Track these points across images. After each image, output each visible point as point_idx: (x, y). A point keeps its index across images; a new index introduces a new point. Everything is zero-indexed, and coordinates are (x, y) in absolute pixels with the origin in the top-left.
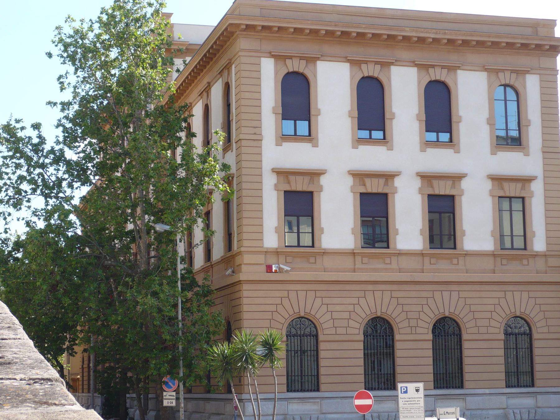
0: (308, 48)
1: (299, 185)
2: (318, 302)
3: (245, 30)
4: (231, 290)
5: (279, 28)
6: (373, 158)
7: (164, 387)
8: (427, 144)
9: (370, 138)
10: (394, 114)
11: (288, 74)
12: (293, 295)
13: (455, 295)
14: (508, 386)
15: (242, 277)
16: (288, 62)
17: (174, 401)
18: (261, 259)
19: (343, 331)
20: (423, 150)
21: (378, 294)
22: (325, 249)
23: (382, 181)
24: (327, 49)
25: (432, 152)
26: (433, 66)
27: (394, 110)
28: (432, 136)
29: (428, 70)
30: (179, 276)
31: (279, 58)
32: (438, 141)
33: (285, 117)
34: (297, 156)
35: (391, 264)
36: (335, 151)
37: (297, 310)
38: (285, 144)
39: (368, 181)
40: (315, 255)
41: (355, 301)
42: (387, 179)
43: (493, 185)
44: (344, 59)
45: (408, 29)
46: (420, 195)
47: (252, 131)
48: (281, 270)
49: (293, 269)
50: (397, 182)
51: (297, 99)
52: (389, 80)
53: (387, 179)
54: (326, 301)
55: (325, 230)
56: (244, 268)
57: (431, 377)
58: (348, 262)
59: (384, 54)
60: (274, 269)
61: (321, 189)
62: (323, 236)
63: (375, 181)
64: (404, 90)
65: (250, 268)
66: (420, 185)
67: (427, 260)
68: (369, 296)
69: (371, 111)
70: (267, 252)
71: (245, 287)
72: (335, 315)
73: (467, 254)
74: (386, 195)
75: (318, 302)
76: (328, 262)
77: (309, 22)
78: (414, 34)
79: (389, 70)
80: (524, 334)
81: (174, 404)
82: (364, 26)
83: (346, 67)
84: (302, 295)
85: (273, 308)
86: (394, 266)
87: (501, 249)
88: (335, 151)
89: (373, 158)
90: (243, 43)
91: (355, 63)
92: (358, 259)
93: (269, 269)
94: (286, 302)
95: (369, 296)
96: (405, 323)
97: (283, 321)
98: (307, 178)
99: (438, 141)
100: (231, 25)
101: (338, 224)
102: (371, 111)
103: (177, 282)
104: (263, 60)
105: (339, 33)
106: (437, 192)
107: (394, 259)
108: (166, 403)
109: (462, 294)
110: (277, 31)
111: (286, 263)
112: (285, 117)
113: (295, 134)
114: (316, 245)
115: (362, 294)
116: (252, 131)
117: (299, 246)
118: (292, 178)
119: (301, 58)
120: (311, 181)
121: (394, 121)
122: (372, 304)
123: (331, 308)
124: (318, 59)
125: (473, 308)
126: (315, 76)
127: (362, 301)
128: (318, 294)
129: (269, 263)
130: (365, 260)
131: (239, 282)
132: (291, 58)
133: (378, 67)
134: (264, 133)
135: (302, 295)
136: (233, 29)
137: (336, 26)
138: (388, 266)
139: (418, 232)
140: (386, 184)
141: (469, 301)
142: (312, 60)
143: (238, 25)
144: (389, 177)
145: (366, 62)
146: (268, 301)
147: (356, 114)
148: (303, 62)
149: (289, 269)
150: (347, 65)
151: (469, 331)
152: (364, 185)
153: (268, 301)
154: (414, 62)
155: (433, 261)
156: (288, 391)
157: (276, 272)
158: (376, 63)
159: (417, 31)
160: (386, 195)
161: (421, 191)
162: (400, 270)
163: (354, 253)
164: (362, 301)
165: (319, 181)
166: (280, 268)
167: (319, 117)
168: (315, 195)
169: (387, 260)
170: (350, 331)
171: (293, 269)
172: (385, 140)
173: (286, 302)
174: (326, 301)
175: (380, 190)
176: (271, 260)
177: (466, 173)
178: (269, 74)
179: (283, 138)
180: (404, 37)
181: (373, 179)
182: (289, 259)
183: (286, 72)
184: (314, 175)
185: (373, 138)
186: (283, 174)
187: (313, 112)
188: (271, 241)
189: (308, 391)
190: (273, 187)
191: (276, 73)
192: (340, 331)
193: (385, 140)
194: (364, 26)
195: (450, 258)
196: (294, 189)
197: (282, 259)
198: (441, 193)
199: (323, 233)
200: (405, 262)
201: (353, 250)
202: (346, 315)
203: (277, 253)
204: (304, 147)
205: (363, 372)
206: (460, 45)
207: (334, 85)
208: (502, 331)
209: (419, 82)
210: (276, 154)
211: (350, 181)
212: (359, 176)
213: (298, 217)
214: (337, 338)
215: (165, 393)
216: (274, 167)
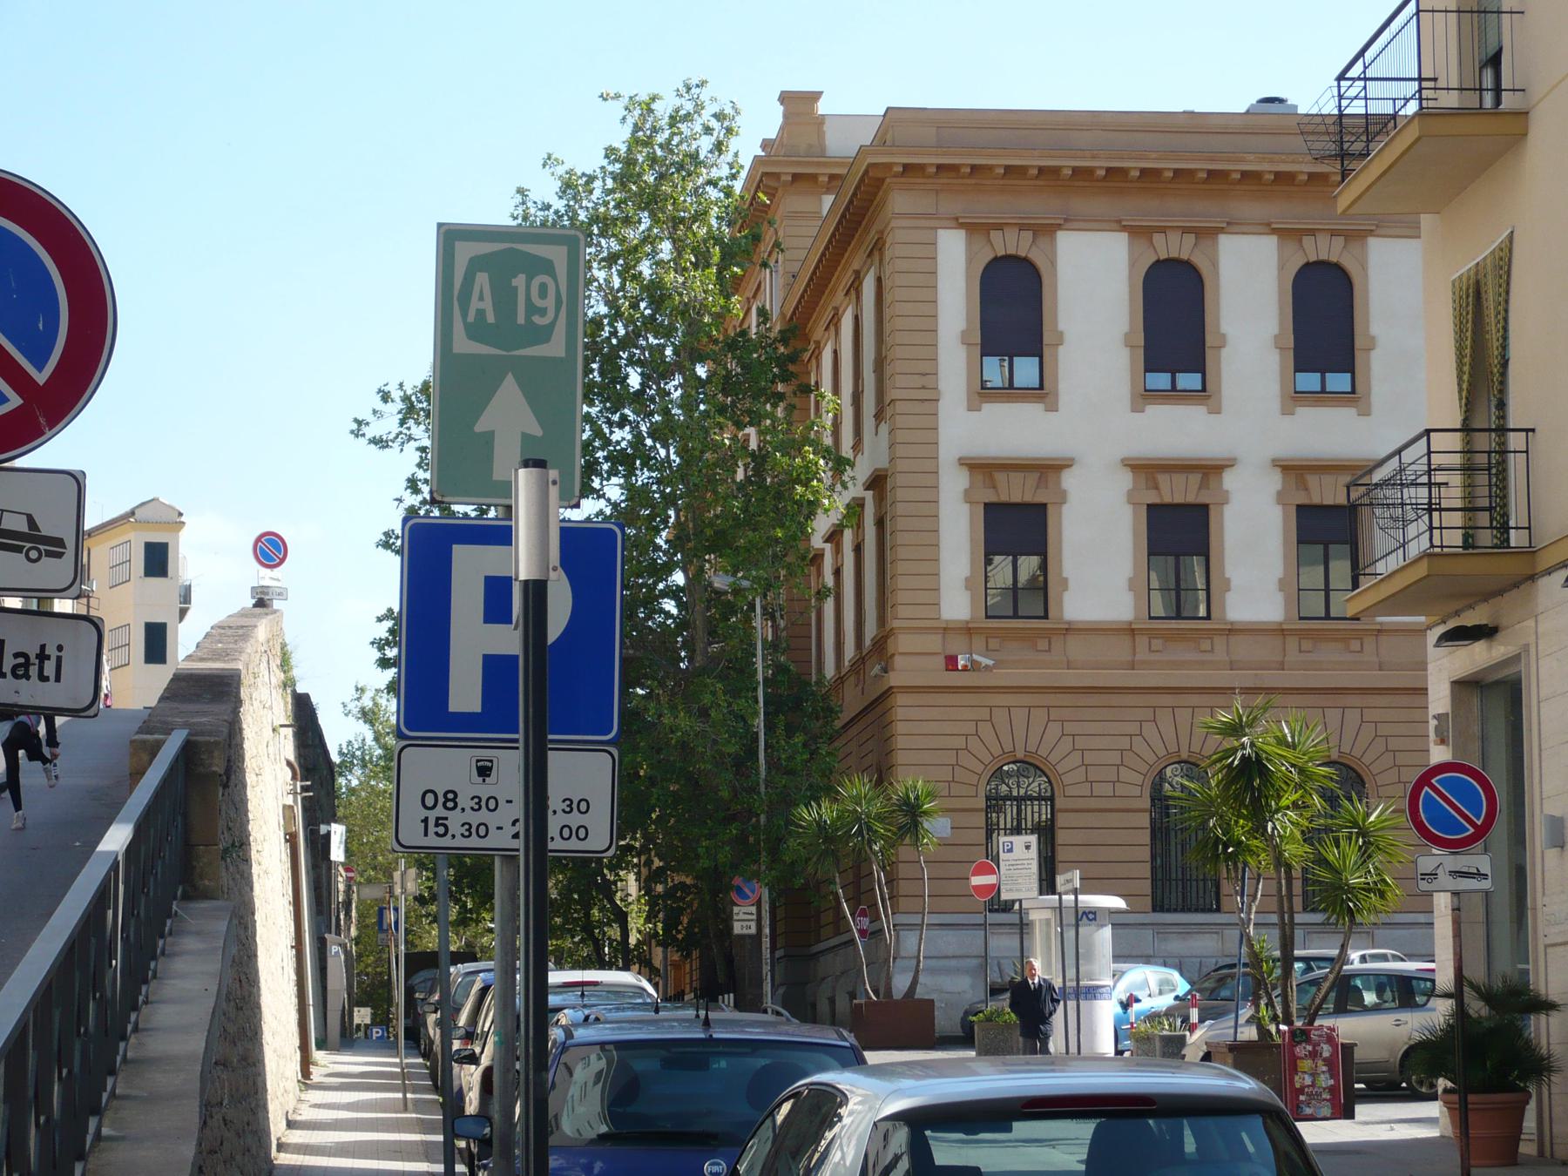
0: (1036, 206)
1: (1016, 491)
2: (1054, 730)
3: (903, 174)
4: (878, 706)
5: (974, 168)
6: (1176, 431)
7: (733, 896)
8: (1296, 398)
9: (1174, 388)
10: (1224, 336)
11: (1158, 263)
12: (1000, 717)
13: (1353, 717)
14: (1158, 907)
15: (894, 679)
16: (995, 236)
17: (753, 925)
18: (933, 643)
19: (1107, 789)
20: (1287, 411)
21: (1184, 715)
22: (1069, 623)
23: (1195, 479)
24: (1079, 205)
25: (1309, 415)
26: (1312, 232)
27: (1225, 327)
28: (1310, 381)
29: (1300, 241)
30: (760, 677)
31: (975, 229)
32: (1323, 391)
33: (987, 350)
34: (1014, 431)
35: (1212, 651)
36: (1093, 417)
37: (1008, 747)
38: (986, 407)
39: (1312, 480)
40: (1049, 634)
41: (1133, 728)
42: (1206, 477)
43: (1135, 482)
44: (1115, 225)
45: (1252, 157)
46: (967, 506)
47: (919, 381)
48: (974, 667)
49: (999, 664)
50: (1230, 480)
51: (1014, 314)
52: (1215, 264)
53: (1206, 477)
54: (1069, 728)
55: (1071, 584)
56: (898, 661)
57: (1146, 886)
58: (1119, 649)
59: (1204, 210)
60: (961, 663)
61: (1062, 497)
62: (1067, 597)
63: (1179, 479)
64: (1248, 287)
65: (913, 663)
66: (1279, 486)
67: (1142, 642)
68: (1165, 719)
69: (1174, 329)
70: (947, 630)
71: (901, 699)
72: (1090, 758)
73: (1070, 630)
74: (1204, 508)
75: (1054, 730)
76: (1075, 648)
77: (1036, 153)
78: (1265, 167)
79: (1364, 247)
80: (1040, 798)
81: (753, 931)
82: (1154, 155)
83: (1269, 244)
84: (1019, 716)
85: (959, 742)
86: (1220, 654)
87: (987, 617)
88: (1093, 417)
89: (1176, 431)
90: (900, 202)
91: (1139, 233)
92: (1142, 642)
93: (951, 662)
94: (986, 730)
95: (1165, 719)
96: (1079, 775)
97: (979, 768)
98: (1033, 478)
99: (1323, 391)
100: (871, 165)
101: (1099, 567)
102: (1174, 329)
103: (755, 689)
104: (941, 232)
105: (1103, 173)
106: (1316, 500)
107: (1219, 642)
108: (738, 929)
109: (1370, 715)
110: (1037, 177)
111: (988, 651)
112: (987, 350)
113: (1011, 386)
114: (1213, 615)
115: (1149, 714)
116: (919, 381)
117: (1328, 617)
118: (1000, 477)
119: (1022, 227)
120: (1042, 482)
121: (1225, 352)
122: (1020, 734)
123: (1081, 743)
124: (1059, 227)
125: (1394, 744)
126: (1053, 263)
127: (1149, 730)
128: (1054, 713)
129: (950, 652)
130: (1157, 644)
131: (889, 692)
132: (1000, 227)
133: (1190, 239)
134: (942, 386)
135: (1019, 716)
136: (880, 175)
137: (1094, 157)
138: (1208, 657)
139: (1273, 586)
140: (1204, 485)
141: (1384, 730)
142: (1045, 231)
143: (889, 166)
144: (1210, 470)
145: (1162, 230)
146: (948, 728)
147: (1140, 340)
148: (1027, 236)
149: (990, 663)
150: (1124, 236)
151: (1070, 791)
152: (1157, 488)
153: (948, 728)
154: (1269, 224)
155: (1306, 645)
156: (1154, 910)
157: (965, 669)
158: (1186, 230)
159: (1271, 161)
160: (1204, 508)
161: (1281, 498)
162: (1232, 666)
163: (1133, 630)
164: (1149, 730)
165: (1058, 483)
166: (973, 662)
167: (1061, 348)
168: (1050, 510)
169: (1206, 645)
170: (1121, 790)
171: (999, 664)
172: (1203, 394)
173: (986, 730)
174: (1069, 728)
175: (1191, 499)
176: (956, 645)
177: (1068, 454)
178: (954, 266)
179: (984, 393)
180: (1245, 174)
181: (1012, 475)
182: (993, 643)
183: (1154, 259)
184: (1049, 469)
185: (1179, 387)
186: (983, 469)
187: (1047, 338)
188: (957, 605)
189: (1196, 911)
190: (961, 495)
191: (970, 261)
192: (1100, 789)
193: (1353, 396)
194: (1154, 155)
195: (1030, 638)
196: (1004, 498)
197: (979, 642)
198: (1326, 502)
199: (1066, 589)
200: (1243, 649)
201: (1131, 623)
202: (1115, 758)
203: (968, 630)
204: (1028, 412)
205: (1148, 875)
206: (1306, 184)
207: (1094, 281)
208: (1147, 794)
209: (1282, 267)
210: (971, 428)
211: (1125, 480)
212: (1146, 470)
213: (1177, 556)
214: (1093, 803)
215: (736, 909)
216: (964, 453)
